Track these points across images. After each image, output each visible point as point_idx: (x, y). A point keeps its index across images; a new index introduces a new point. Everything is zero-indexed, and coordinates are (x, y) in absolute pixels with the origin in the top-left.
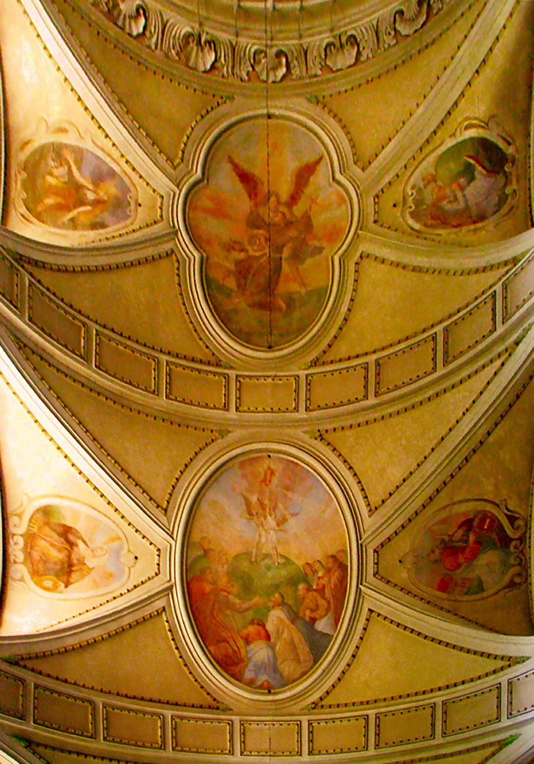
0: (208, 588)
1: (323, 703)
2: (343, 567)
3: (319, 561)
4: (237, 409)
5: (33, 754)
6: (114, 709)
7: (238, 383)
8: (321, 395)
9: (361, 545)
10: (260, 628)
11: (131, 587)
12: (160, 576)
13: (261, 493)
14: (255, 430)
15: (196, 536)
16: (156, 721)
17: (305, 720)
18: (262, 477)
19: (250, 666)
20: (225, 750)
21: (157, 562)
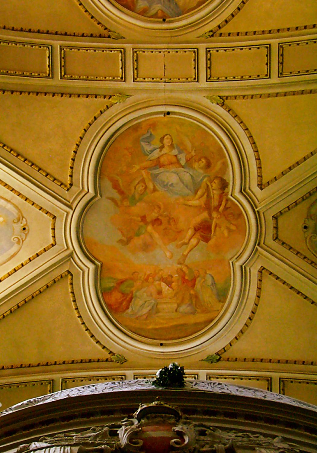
1: (222, 31)
17: (202, 48)
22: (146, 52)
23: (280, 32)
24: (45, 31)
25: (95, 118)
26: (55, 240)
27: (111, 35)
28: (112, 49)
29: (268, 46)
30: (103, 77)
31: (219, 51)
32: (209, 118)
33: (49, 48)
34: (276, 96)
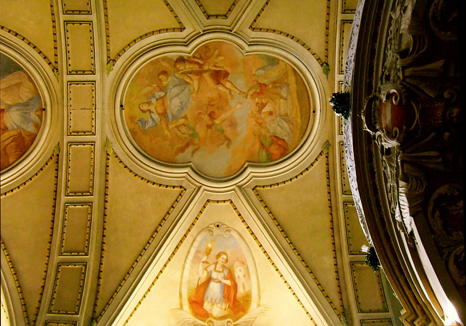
1: (53, 62)
4: (94, 134)
5: (102, 316)
6: (63, 246)
16: (69, 209)
19: (24, 126)
25: (126, 167)
27: (56, 154)
30: (91, 161)
31: (70, 64)
33: (68, 206)
34: (107, 16)
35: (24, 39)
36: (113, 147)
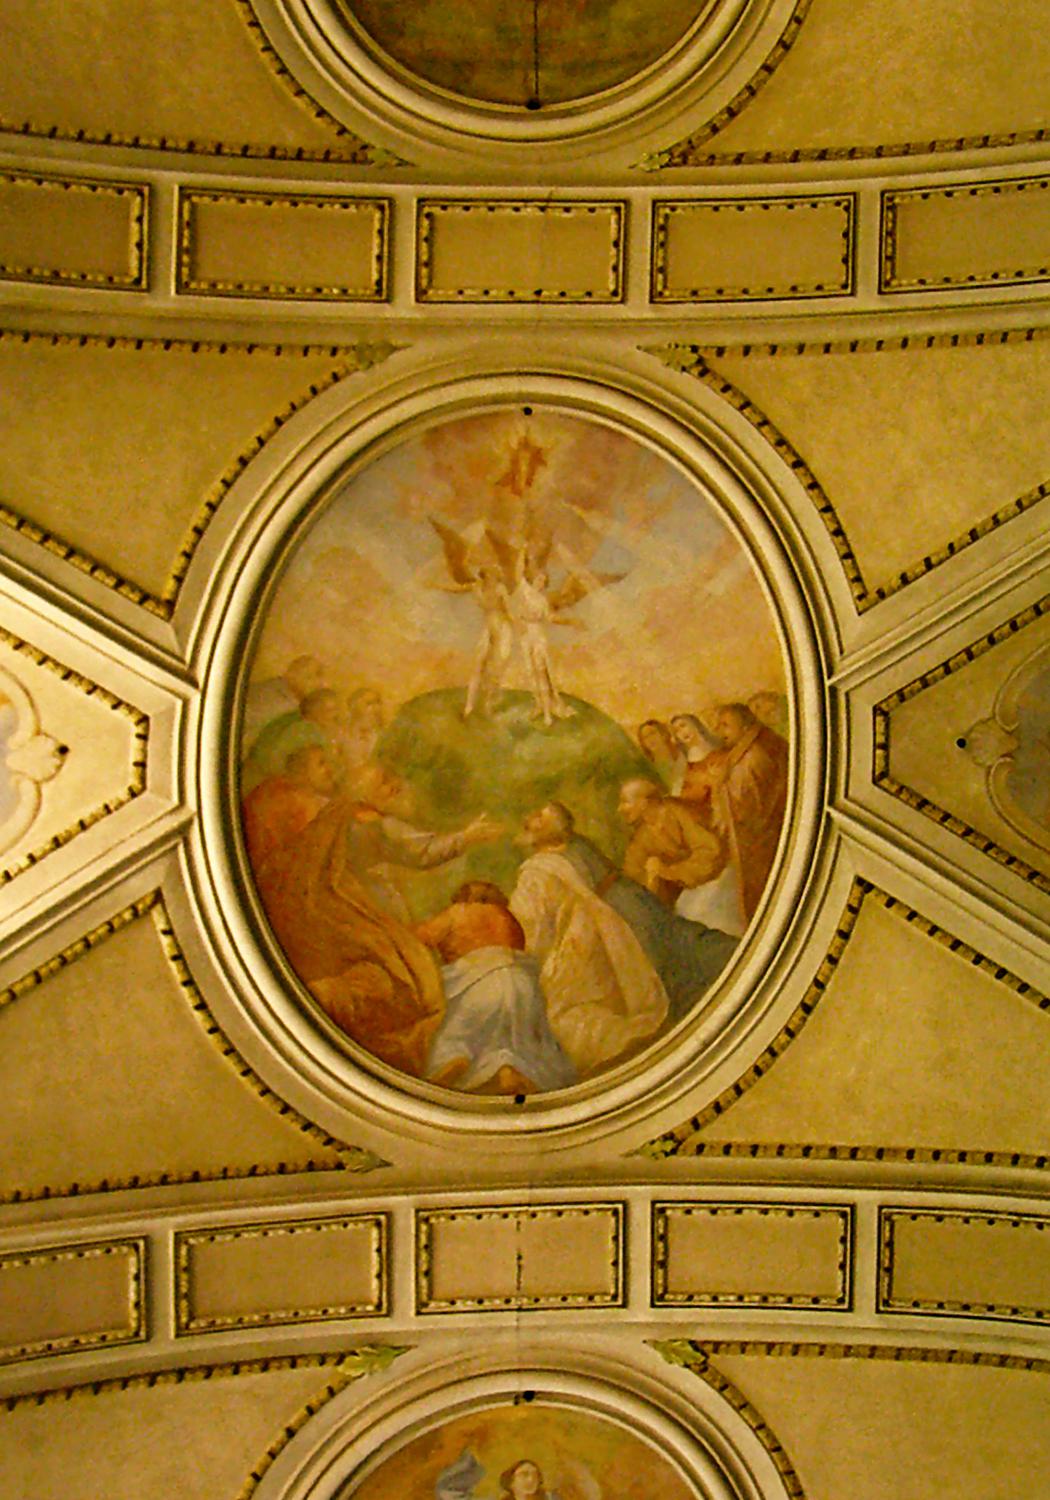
0: (312, 806)
1: (704, 1136)
2: (773, 747)
3: (693, 718)
4: (421, 295)
7: (426, 223)
8: (701, 255)
9: (833, 690)
10: (489, 908)
11: (38, 841)
12: (146, 795)
13: (499, 514)
14: (476, 339)
15: (274, 659)
17: (640, 1198)
18: (505, 466)
19: (455, 1026)
20: (367, 1303)
21: (134, 756)
22: (459, 1219)
23: (884, 1158)
24: (126, 1182)
25: (291, 1433)
26: (143, 779)
27: (344, 1161)
28: (346, 1219)
29: (848, 1209)
30: (317, 1310)
31: (694, 1212)
32: (658, 1409)
33: (136, 1247)
34: (871, 1356)
35: (791, 1033)
36: (371, 1374)
